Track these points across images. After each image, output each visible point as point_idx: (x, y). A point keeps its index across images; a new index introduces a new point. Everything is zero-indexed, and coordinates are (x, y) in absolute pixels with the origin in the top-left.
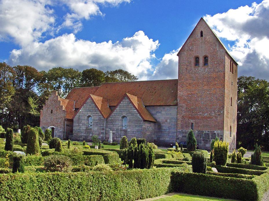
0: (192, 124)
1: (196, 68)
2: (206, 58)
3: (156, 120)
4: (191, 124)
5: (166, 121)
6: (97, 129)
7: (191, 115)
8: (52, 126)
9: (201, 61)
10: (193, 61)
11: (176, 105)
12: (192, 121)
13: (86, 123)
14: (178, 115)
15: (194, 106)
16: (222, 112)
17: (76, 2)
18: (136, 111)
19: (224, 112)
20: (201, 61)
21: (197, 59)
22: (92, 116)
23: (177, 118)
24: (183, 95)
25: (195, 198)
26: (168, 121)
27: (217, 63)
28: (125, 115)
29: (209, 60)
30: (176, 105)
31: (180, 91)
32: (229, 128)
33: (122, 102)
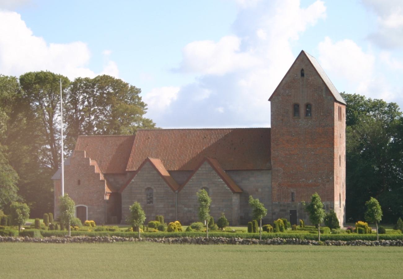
0: (292, 193)
1: (296, 120)
2: (308, 106)
3: (242, 190)
4: (291, 194)
5: (257, 191)
6: (162, 206)
7: (291, 182)
8: (82, 204)
9: (302, 111)
10: (291, 109)
11: (270, 169)
12: (292, 190)
13: (143, 198)
14: (273, 183)
15: (294, 170)
16: (331, 178)
17: (373, 207)
18: (222, 180)
19: (333, 178)
20: (302, 111)
21: (296, 107)
22: (153, 187)
23: (272, 186)
24: (279, 155)
25: (344, 157)
26: (260, 190)
27: (323, 115)
28: (149, 186)
29: (313, 109)
30: (270, 169)
31: (274, 150)
32: (339, 195)
33: (200, 169)
